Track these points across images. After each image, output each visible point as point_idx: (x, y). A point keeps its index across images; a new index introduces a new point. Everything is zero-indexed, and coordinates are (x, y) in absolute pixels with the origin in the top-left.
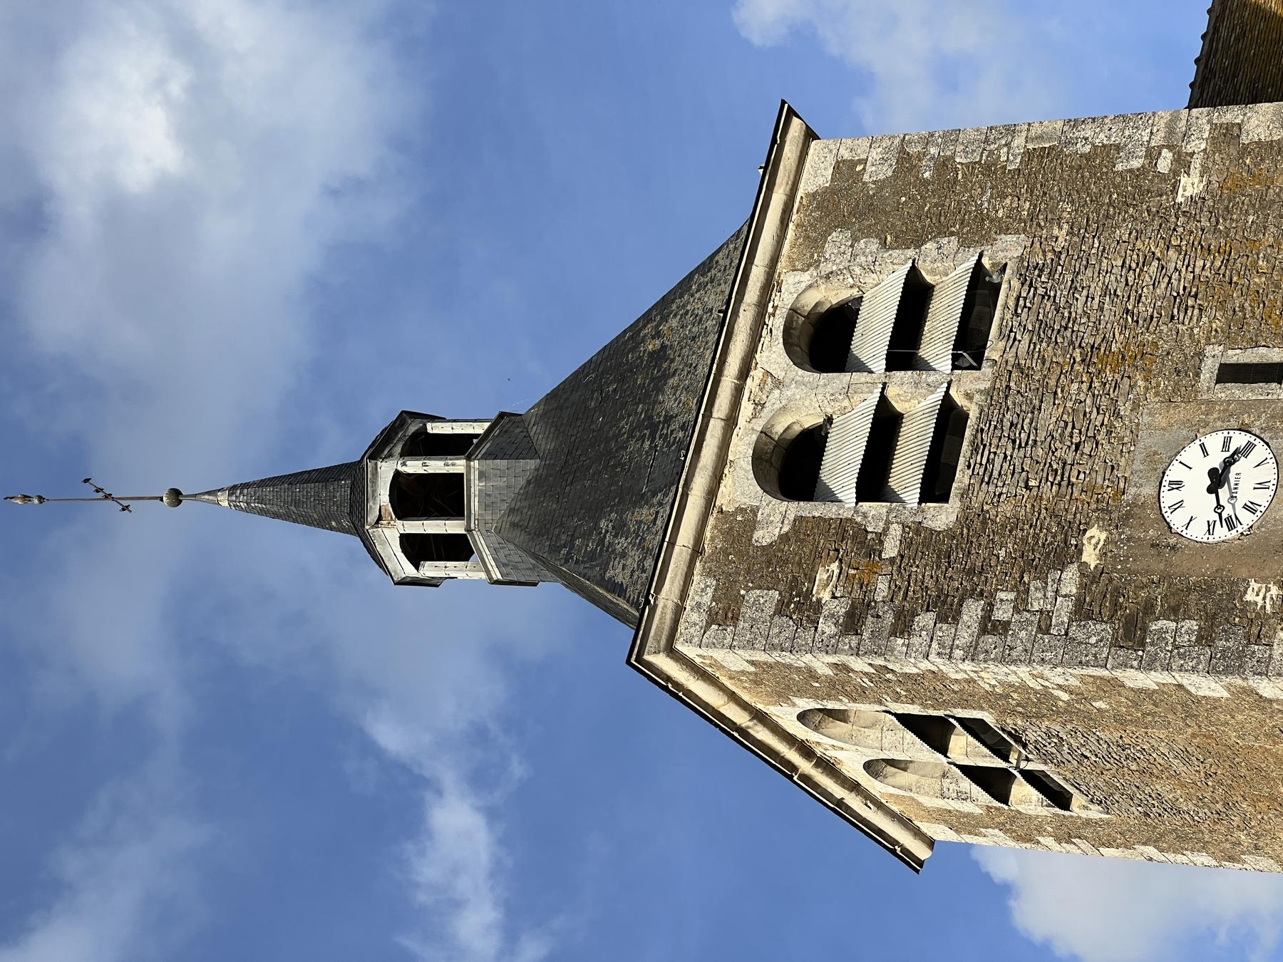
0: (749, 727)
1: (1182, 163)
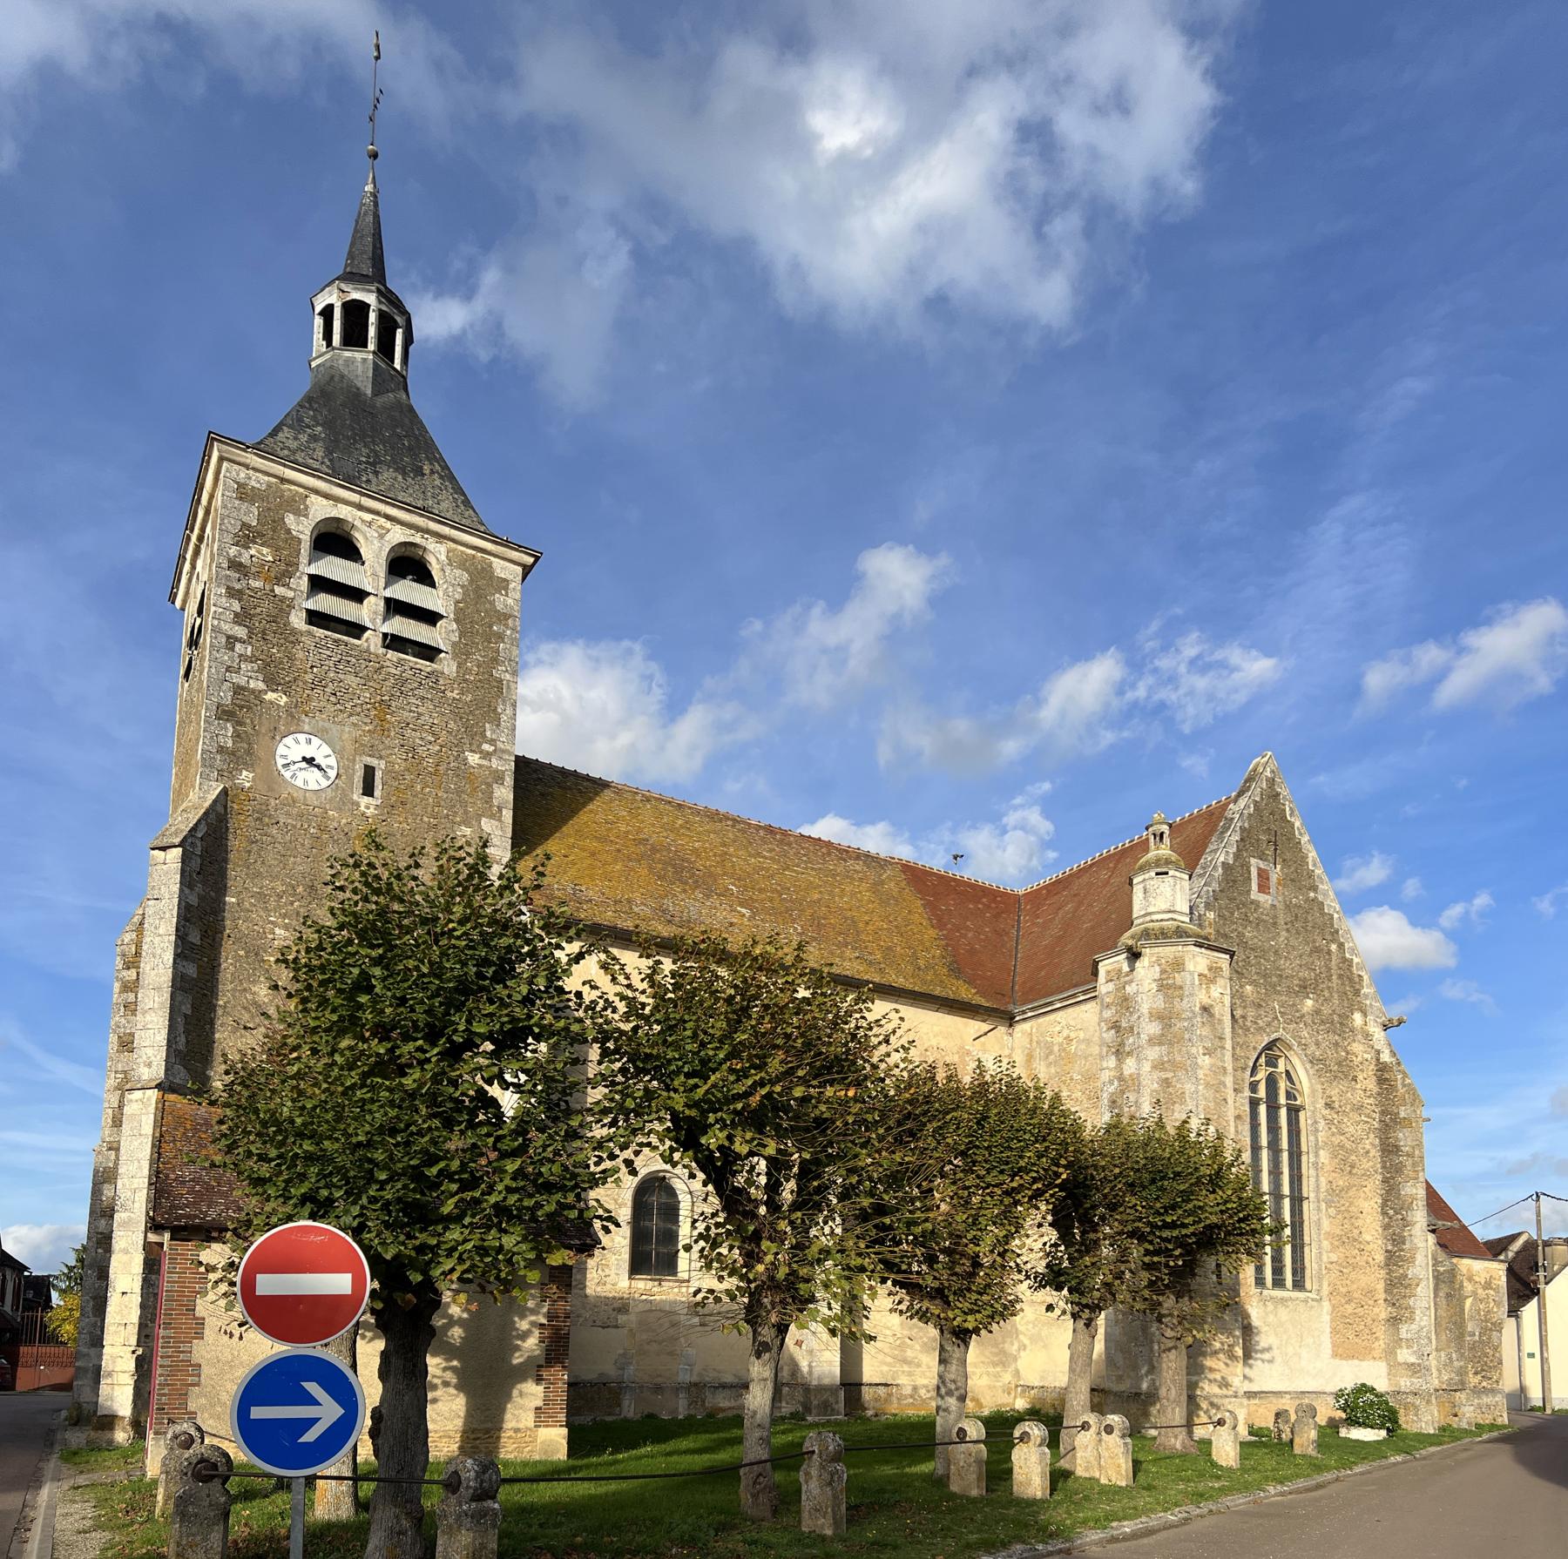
1: (486, 755)
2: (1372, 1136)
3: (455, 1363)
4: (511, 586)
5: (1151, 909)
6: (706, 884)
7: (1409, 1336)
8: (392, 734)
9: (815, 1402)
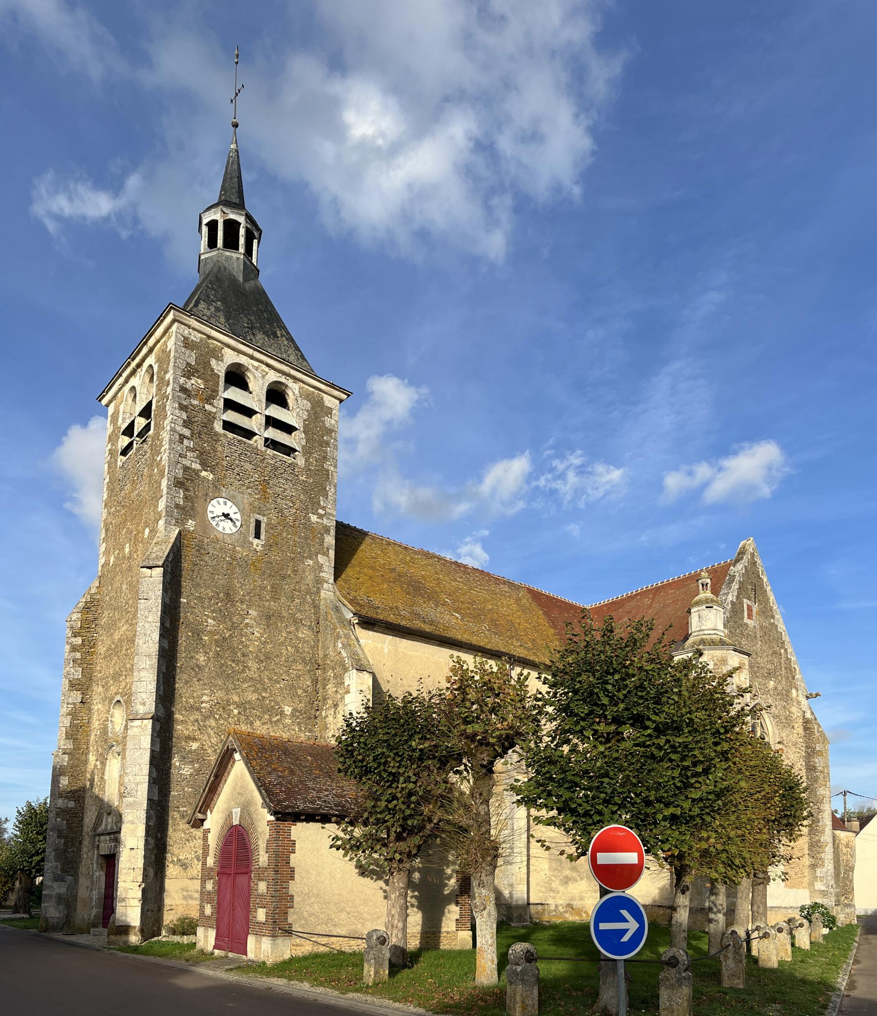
1: (321, 516)
2: (801, 760)
3: (416, 893)
4: (333, 412)
5: (703, 628)
6: (432, 597)
7: (821, 875)
8: (270, 501)
9: (515, 915)
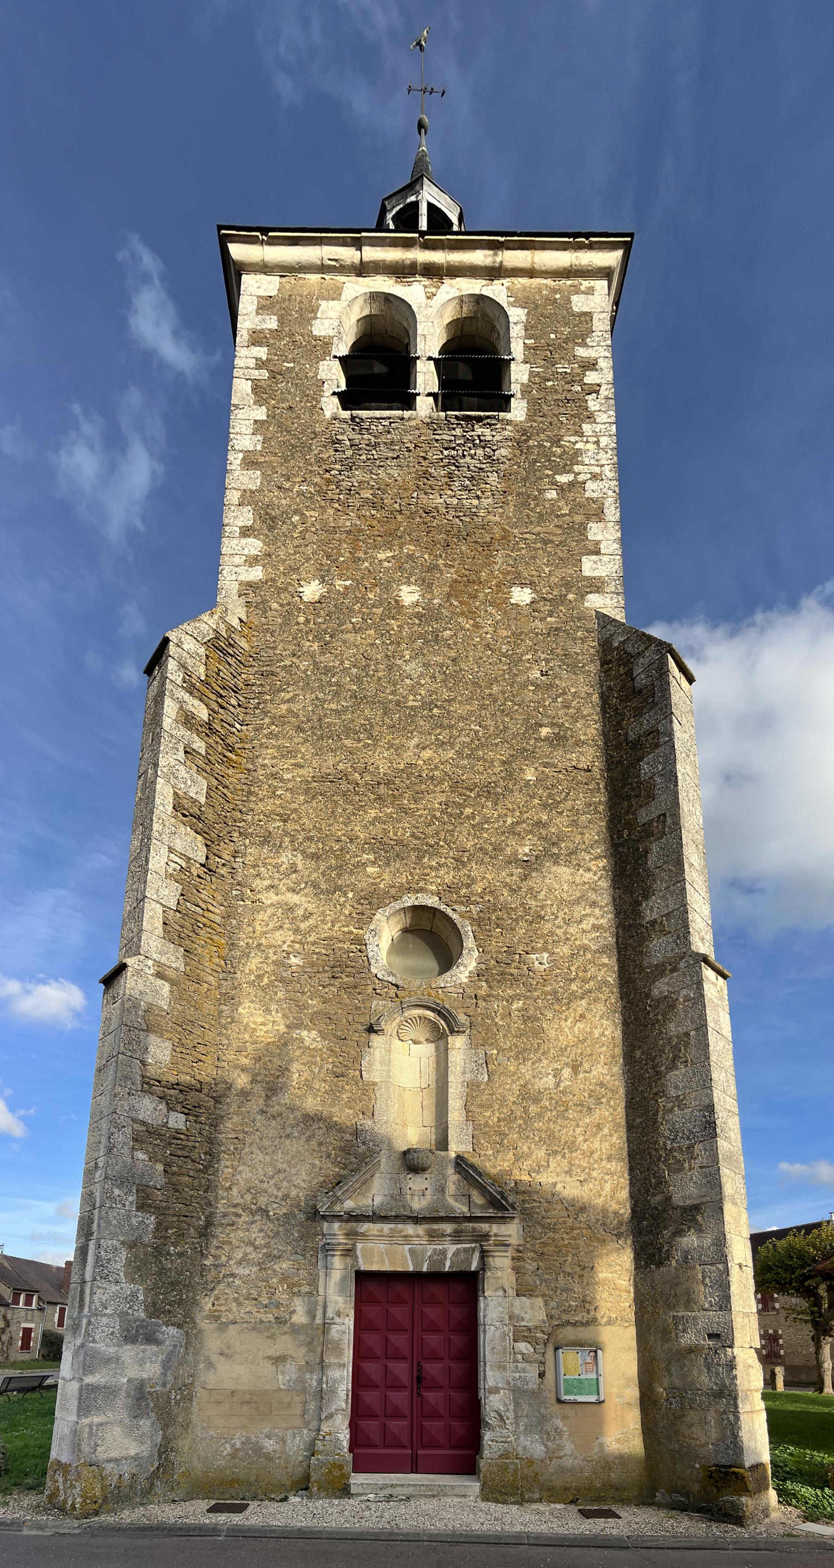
0: (496, 255)
